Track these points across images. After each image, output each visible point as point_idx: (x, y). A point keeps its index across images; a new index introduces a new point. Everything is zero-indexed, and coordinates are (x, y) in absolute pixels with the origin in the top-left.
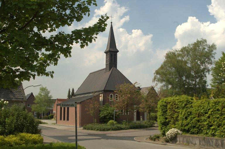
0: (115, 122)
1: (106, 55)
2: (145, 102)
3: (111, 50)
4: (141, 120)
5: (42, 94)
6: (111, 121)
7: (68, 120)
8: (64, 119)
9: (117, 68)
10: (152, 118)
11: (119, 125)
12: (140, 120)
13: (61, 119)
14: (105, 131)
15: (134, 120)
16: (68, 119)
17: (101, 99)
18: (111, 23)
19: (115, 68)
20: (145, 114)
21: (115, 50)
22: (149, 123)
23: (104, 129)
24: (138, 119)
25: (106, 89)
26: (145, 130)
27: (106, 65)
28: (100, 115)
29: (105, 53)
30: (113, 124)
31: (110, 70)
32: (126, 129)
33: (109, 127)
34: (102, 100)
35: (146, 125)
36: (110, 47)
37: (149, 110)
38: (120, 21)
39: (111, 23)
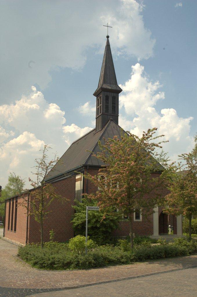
0: (88, 242)
1: (98, 100)
2: (179, 189)
3: (105, 86)
4: (170, 233)
5: (12, 187)
6: (78, 238)
7: (16, 231)
8: (12, 230)
9: (119, 124)
10: (185, 180)
11: (104, 251)
12: (167, 231)
13: (9, 229)
14: (56, 269)
15: (152, 234)
16: (15, 230)
17: (79, 186)
18: (108, 37)
19: (113, 124)
20: (179, 218)
21: (114, 88)
22: (188, 243)
23: (53, 263)
24: (163, 230)
25: (90, 163)
26: (180, 266)
27: (96, 118)
28: (74, 221)
29: (94, 95)
30: (80, 246)
31: (103, 127)
32: (123, 263)
33: (70, 256)
34: (82, 189)
35: (181, 248)
36: (105, 82)
37: (189, 210)
38: (152, 99)
39: (108, 37)
